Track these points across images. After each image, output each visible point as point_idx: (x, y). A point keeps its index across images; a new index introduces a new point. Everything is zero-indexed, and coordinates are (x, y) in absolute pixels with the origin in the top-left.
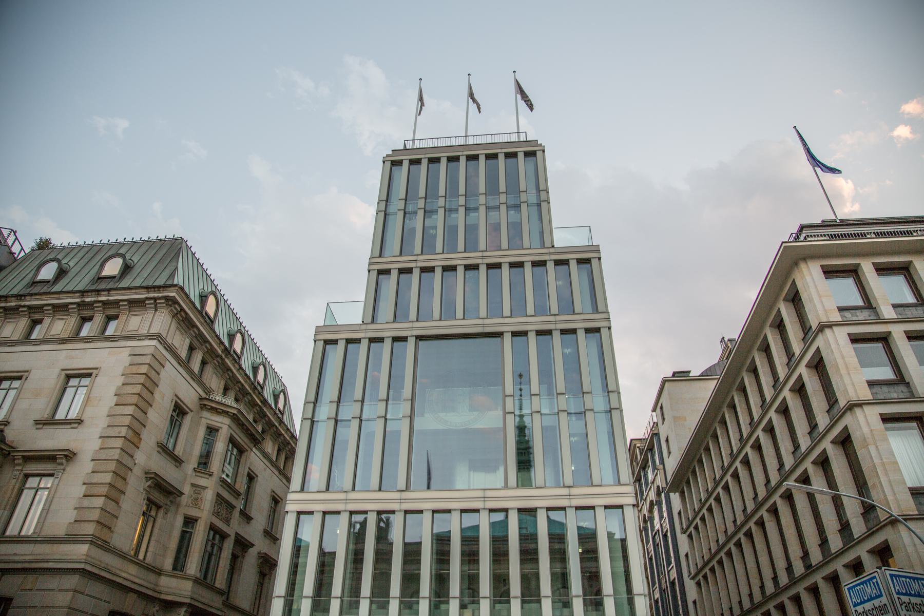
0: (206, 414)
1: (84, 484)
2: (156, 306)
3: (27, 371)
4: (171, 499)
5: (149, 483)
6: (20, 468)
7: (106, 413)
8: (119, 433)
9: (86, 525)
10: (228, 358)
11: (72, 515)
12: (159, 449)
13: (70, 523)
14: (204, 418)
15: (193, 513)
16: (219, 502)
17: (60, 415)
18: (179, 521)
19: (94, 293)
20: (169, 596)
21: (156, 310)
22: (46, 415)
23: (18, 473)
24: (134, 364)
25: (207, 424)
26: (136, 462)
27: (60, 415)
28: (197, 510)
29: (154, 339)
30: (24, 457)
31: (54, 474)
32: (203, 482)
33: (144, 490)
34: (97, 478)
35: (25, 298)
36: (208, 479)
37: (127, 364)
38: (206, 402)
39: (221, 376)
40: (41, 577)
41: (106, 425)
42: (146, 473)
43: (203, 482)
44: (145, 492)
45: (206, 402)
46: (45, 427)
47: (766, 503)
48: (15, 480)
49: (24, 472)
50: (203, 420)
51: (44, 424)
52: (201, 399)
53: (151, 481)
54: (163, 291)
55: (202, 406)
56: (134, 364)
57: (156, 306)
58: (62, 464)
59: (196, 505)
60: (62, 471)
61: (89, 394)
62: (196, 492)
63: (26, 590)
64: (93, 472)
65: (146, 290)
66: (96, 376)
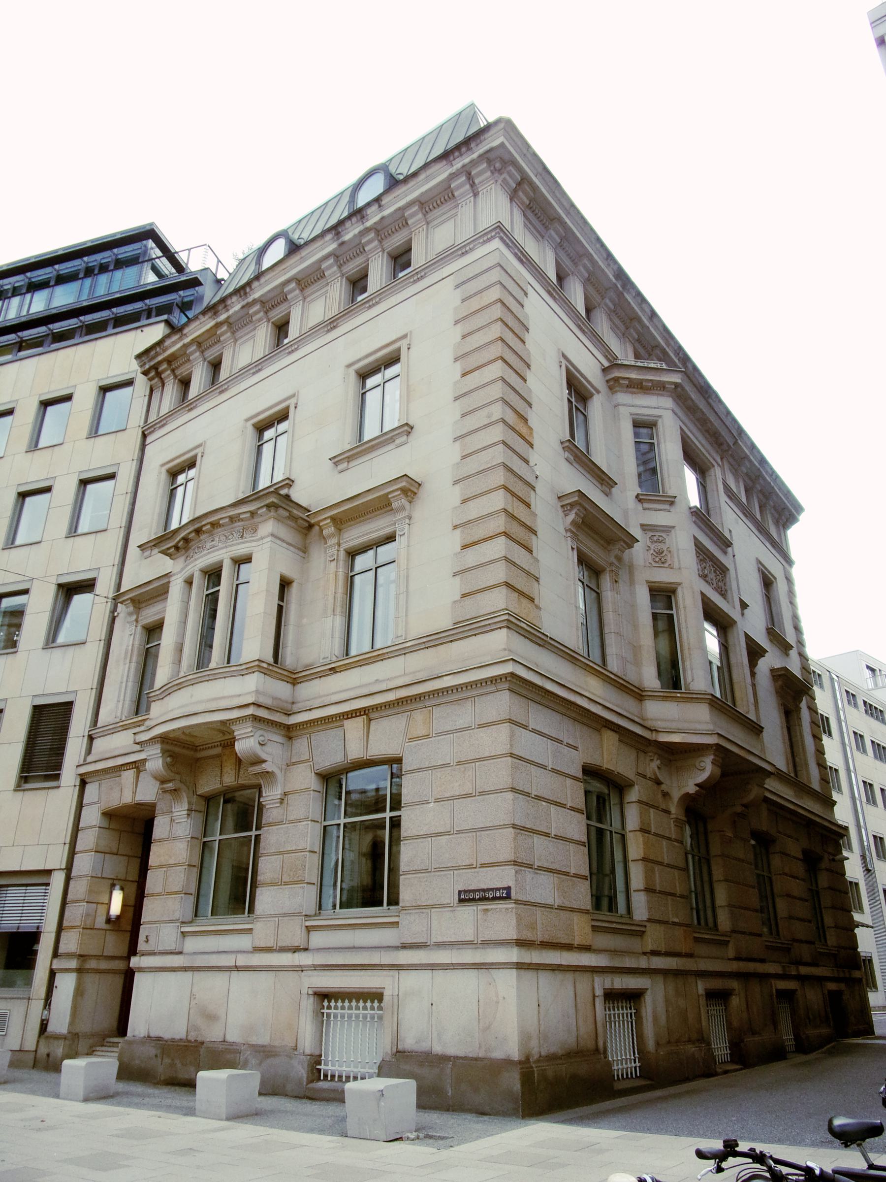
0: (622, 397)
1: (455, 527)
2: (473, 185)
3: (293, 396)
4: (616, 552)
5: (572, 517)
6: (335, 540)
7: (451, 397)
8: (489, 417)
9: (487, 595)
10: (629, 292)
11: (453, 588)
12: (567, 454)
13: (455, 602)
14: (621, 405)
15: (663, 576)
16: (701, 557)
17: (371, 431)
18: (643, 596)
19: (354, 219)
20: (673, 735)
21: (476, 195)
22: (345, 442)
23: (334, 550)
24: (470, 297)
25: (631, 414)
26: (538, 473)
27: (371, 431)
28: (669, 570)
29: (493, 238)
30: (333, 519)
31: (395, 532)
32: (660, 518)
33: (566, 531)
34: (475, 509)
35: (251, 287)
36: (669, 511)
37: (458, 302)
38: (616, 373)
39: (624, 334)
40: (437, 711)
41: (459, 416)
42: (559, 498)
43: (660, 518)
44: (569, 534)
45: (616, 373)
46: (352, 464)
47: (177, 1088)
48: (333, 564)
49: (345, 546)
50: (622, 409)
51: (349, 459)
52: (605, 370)
53: (574, 512)
54: (477, 145)
55: (611, 383)
56: (470, 297)
57: (473, 185)
58: (403, 508)
59: (663, 563)
60: (407, 521)
61: (408, 381)
62: (655, 538)
63: (418, 738)
64: (464, 501)
65: (444, 162)
66: (409, 348)
